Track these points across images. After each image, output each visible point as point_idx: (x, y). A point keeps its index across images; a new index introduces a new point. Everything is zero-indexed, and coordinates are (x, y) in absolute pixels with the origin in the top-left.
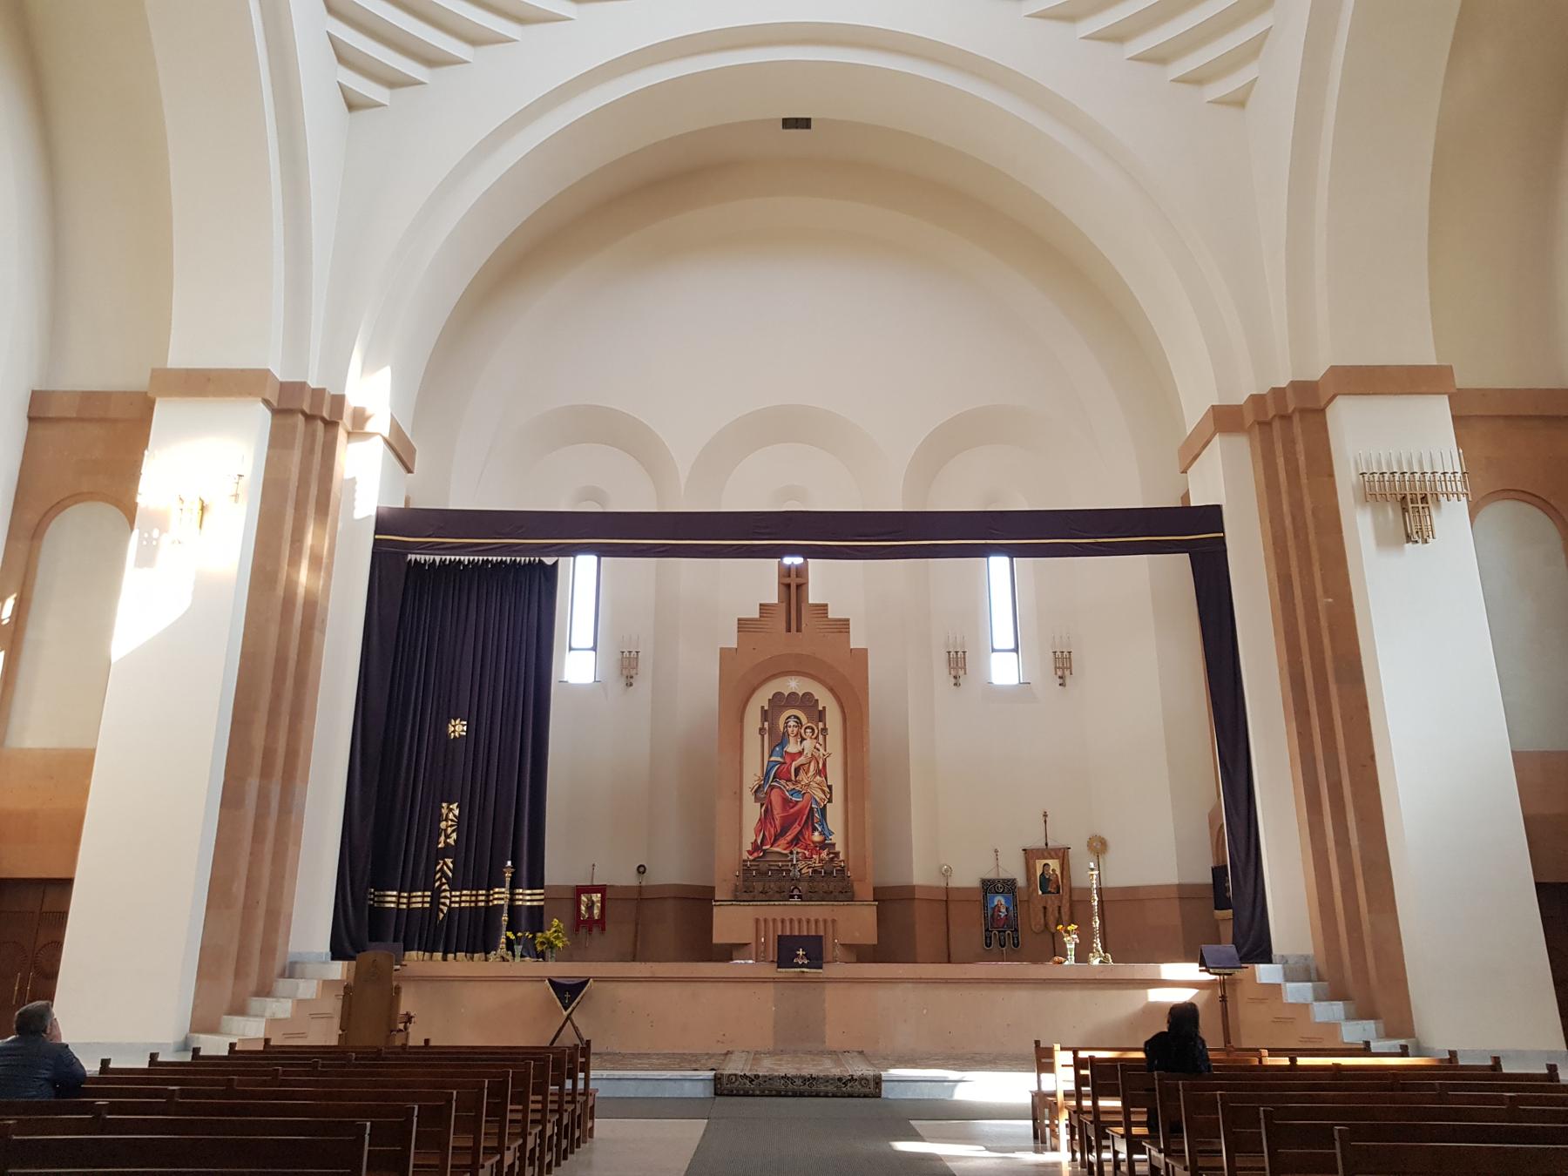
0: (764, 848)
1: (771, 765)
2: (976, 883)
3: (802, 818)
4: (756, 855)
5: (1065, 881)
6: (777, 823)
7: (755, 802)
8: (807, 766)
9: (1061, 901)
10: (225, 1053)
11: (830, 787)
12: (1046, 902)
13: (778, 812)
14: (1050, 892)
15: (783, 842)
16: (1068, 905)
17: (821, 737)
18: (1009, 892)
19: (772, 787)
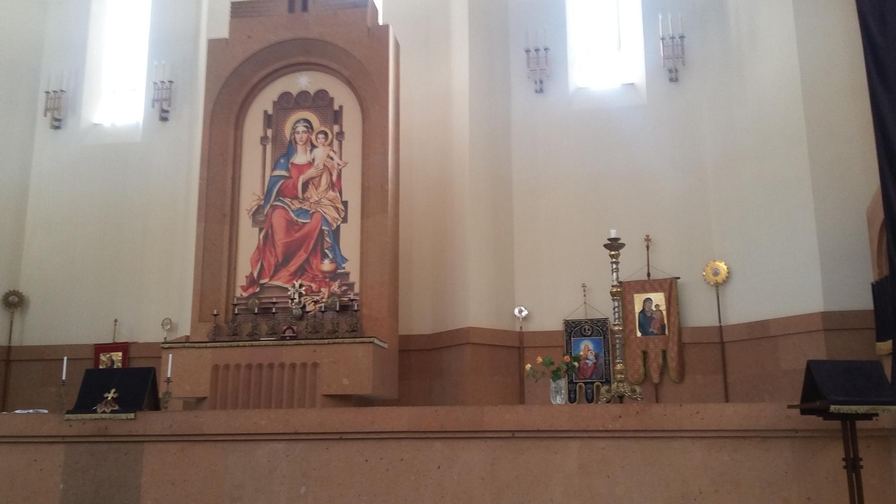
0: (262, 282)
1: (274, 180)
2: (559, 326)
3: (309, 244)
4: (251, 291)
5: (672, 319)
6: (279, 250)
7: (253, 226)
8: (317, 179)
9: (667, 344)
10: (846, 470)
11: (345, 204)
12: (647, 346)
13: (280, 238)
14: (652, 333)
15: (285, 273)
16: (676, 348)
17: (336, 143)
18: (599, 334)
19: (274, 208)
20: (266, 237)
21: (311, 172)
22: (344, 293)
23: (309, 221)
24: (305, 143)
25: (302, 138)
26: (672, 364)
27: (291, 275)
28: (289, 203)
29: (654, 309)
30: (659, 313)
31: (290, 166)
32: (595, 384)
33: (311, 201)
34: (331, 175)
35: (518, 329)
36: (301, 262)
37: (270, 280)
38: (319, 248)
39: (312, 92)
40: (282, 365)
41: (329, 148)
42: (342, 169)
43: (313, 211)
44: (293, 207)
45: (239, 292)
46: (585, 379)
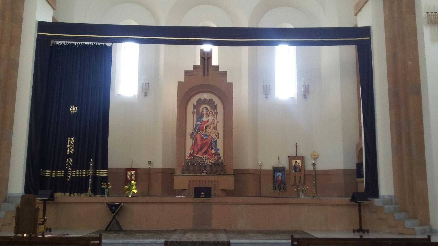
0: (194, 155)
1: (197, 125)
3: (208, 145)
4: (191, 158)
6: (199, 146)
7: (191, 139)
8: (210, 126)
11: (218, 133)
13: (199, 142)
15: (201, 153)
17: (215, 115)
19: (197, 133)
20: (195, 142)
21: (208, 123)
22: (218, 160)
23: (208, 138)
24: (206, 115)
25: (205, 113)
26: (302, 180)
27: (202, 153)
28: (202, 132)
29: (298, 165)
30: (299, 166)
31: (202, 121)
34: (214, 125)
35: (259, 169)
36: (205, 150)
37: (196, 155)
38: (211, 146)
40: (209, 181)
41: (213, 116)
42: (218, 123)
43: (209, 135)
44: (202, 133)
45: (187, 158)
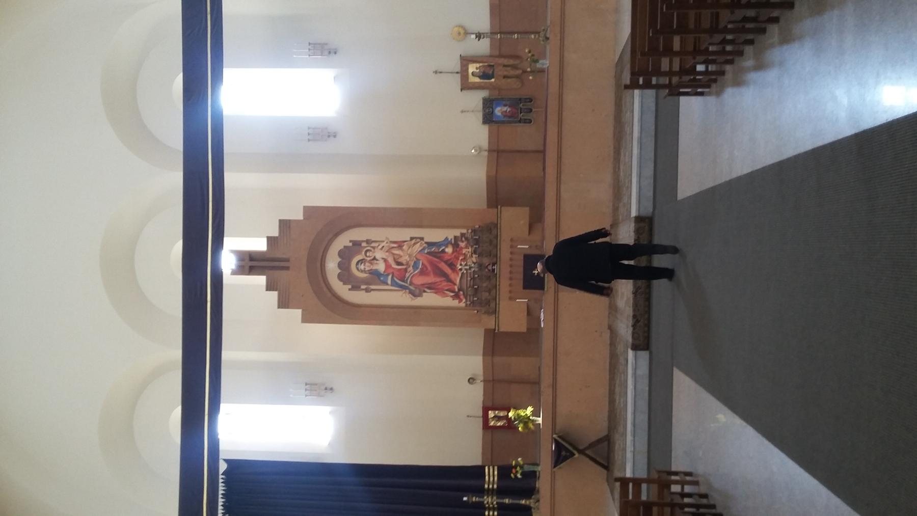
0: (457, 290)
1: (394, 283)
4: (462, 297)
6: (438, 279)
11: (412, 239)
14: (493, 72)
15: (452, 276)
17: (373, 245)
19: (411, 283)
20: (429, 288)
21: (391, 260)
22: (467, 239)
24: (372, 264)
25: (368, 266)
26: (511, 62)
28: (409, 274)
29: (478, 70)
31: (385, 274)
32: (522, 107)
33: (408, 260)
34: (393, 247)
35: (486, 153)
38: (439, 255)
39: (339, 260)
40: (511, 259)
41: (376, 249)
43: (415, 259)
44: (411, 272)
45: (463, 304)
46: (518, 113)
